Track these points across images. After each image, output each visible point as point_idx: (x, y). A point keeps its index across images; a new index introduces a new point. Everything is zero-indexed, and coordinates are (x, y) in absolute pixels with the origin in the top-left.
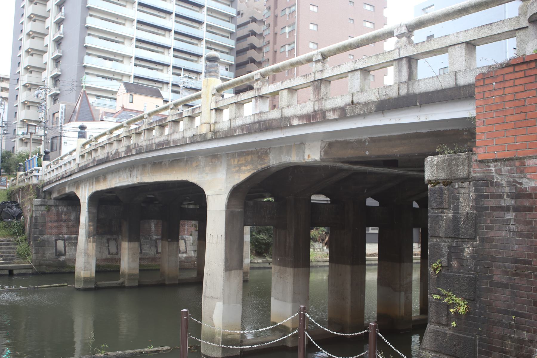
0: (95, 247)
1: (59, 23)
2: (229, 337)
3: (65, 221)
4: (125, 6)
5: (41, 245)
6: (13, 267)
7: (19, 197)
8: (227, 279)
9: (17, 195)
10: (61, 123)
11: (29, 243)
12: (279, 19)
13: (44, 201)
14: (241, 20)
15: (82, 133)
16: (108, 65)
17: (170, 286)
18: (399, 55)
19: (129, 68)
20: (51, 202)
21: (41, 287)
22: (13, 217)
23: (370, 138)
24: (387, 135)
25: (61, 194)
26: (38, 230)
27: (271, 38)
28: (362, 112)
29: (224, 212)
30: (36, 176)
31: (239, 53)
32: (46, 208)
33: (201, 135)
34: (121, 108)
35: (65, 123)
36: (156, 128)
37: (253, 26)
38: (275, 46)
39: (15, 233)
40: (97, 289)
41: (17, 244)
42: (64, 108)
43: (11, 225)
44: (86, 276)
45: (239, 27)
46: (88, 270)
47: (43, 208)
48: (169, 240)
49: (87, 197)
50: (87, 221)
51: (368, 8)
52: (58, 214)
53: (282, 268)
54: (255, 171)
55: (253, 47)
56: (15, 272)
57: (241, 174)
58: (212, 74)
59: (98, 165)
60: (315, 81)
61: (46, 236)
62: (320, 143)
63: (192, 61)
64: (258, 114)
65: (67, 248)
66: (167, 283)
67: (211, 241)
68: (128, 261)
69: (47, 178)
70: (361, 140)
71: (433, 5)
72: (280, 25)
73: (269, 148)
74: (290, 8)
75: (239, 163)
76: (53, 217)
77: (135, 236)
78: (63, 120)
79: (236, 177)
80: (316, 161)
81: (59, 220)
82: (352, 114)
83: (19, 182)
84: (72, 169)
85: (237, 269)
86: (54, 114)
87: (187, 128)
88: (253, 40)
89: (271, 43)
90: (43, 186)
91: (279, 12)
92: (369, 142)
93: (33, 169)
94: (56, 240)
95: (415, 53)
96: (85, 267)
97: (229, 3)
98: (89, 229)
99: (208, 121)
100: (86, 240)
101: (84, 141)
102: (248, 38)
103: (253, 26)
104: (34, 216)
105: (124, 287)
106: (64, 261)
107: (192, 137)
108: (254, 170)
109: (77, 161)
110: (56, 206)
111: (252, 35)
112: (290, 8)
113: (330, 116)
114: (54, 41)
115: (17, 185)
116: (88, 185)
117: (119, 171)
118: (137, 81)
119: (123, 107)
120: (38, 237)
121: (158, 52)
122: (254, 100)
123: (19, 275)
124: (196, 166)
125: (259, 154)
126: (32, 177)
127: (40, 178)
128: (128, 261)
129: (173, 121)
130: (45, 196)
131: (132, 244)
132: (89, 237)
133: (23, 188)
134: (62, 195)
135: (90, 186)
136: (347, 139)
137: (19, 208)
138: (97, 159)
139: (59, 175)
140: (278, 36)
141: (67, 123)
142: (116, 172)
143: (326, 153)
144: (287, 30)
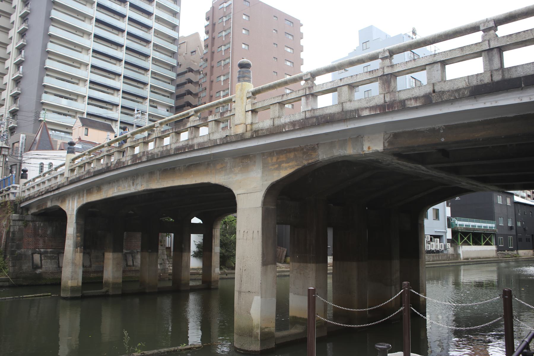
0: (82, 257)
1: (18, 65)
2: (266, 330)
3: (42, 236)
4: (81, 52)
5: (18, 259)
8: (264, 273)
10: (21, 152)
11: (5, 257)
12: (215, 69)
14: (180, 70)
15: (71, 149)
16: (64, 103)
18: (489, 46)
19: (83, 106)
20: (29, 218)
21: (26, 297)
23: (447, 127)
24: (466, 122)
25: (41, 208)
27: (207, 85)
28: (452, 98)
29: (261, 209)
30: (13, 193)
31: (179, 97)
33: (236, 135)
34: (77, 140)
35: (25, 152)
36: (171, 135)
37: (190, 76)
38: (211, 92)
40: (83, 297)
42: (25, 138)
44: (74, 285)
45: (178, 75)
47: (20, 223)
48: (150, 251)
49: (75, 210)
50: (75, 232)
51: (288, 64)
53: (302, 264)
54: (300, 167)
55: (189, 93)
57: (281, 171)
58: (246, 79)
59: (94, 176)
60: (384, 75)
61: (23, 250)
62: (383, 135)
63: (138, 102)
64: (311, 111)
65: (43, 262)
66: (147, 291)
67: (245, 238)
68: (111, 270)
70: (434, 128)
72: (216, 74)
73: (317, 144)
74: (224, 60)
75: (279, 160)
77: (117, 248)
78: (23, 149)
79: (275, 174)
80: (377, 152)
81: (35, 234)
82: (440, 100)
84: (59, 184)
85: (272, 264)
86: (13, 144)
87: (213, 131)
88: (190, 87)
89: (208, 89)
90: (21, 202)
91: (215, 63)
92: (443, 129)
94: (33, 254)
95: (508, 43)
96: (72, 277)
97: (170, 55)
99: (244, 122)
100: (73, 250)
101: (73, 156)
102: (186, 86)
103: (190, 76)
104: (12, 230)
105: (108, 296)
106: (40, 274)
107: (224, 138)
108: (298, 165)
109: (66, 175)
111: (189, 83)
112: (224, 60)
113: (412, 104)
114: (14, 80)
116: (76, 198)
117: (110, 183)
118: (89, 118)
119: (80, 139)
120: (15, 251)
121: (108, 93)
122: (303, 99)
124: (222, 168)
125: (305, 150)
126: (8, 194)
127: (17, 195)
128: (111, 270)
129: (195, 127)
131: (116, 255)
132: (77, 248)
134: (42, 210)
135: (79, 198)
136: (417, 128)
138: (92, 170)
140: (214, 83)
141: (27, 151)
143: (390, 143)
144: (222, 78)
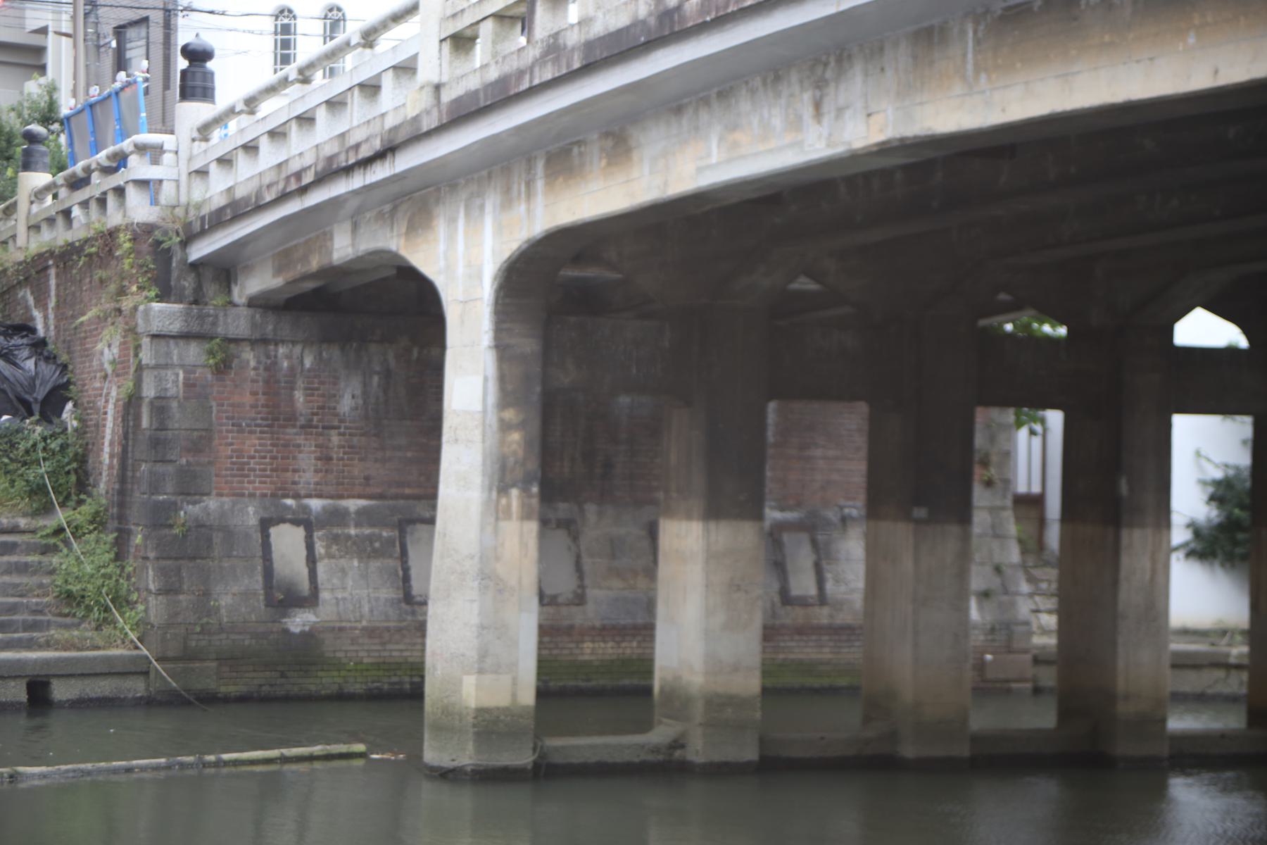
3: (308, 426)
5: (189, 550)
6: (47, 662)
7: (41, 302)
9: (27, 295)
13: (201, 317)
17: (926, 767)
20: (238, 323)
21: (236, 763)
22: (22, 407)
25: (300, 269)
26: (170, 468)
30: (143, 184)
32: (211, 353)
39: (37, 490)
40: (546, 773)
41: (54, 549)
43: (13, 445)
46: (496, 670)
47: (194, 353)
48: (920, 512)
50: (492, 399)
52: (275, 387)
56: (60, 691)
59: (589, 68)
61: (212, 503)
65: (321, 568)
66: (909, 751)
69: (216, 190)
71: (412, 10)
76: (248, 399)
77: (734, 487)
81: (277, 416)
83: (34, 228)
84: (390, 122)
93: (127, 145)
94: (265, 525)
96: (483, 655)
98: (502, 442)
106: (309, 637)
109: (428, 71)
110: (264, 341)
115: (21, 241)
116: (491, 201)
120: (173, 507)
123: (81, 704)
126: (120, 191)
130: (199, 289)
132: (503, 489)
133: (66, 256)
135: (507, 203)
137: (50, 359)
139: (295, 166)
142: (706, 101)
